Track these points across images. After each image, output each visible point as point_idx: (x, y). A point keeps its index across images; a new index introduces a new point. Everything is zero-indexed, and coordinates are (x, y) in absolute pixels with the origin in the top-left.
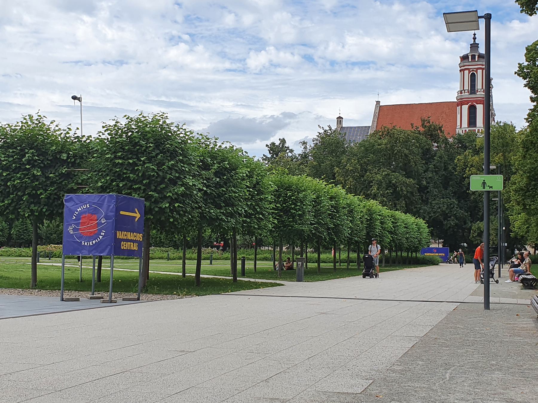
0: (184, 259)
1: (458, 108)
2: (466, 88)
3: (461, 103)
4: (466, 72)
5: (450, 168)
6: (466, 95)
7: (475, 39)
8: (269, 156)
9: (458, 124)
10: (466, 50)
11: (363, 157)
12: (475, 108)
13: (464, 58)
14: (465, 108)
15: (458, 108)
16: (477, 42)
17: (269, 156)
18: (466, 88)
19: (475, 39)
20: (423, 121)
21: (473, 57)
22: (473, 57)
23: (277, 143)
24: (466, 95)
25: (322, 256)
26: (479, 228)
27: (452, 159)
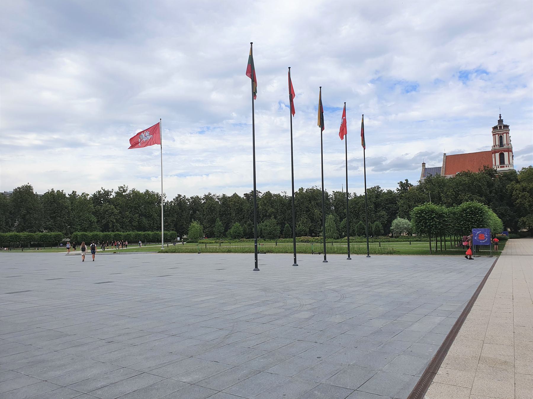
0: (368, 242)
1: (493, 155)
2: (497, 144)
3: (494, 152)
4: (497, 136)
5: (504, 191)
6: (498, 147)
7: (500, 117)
8: (400, 188)
9: (494, 163)
10: (496, 124)
11: (455, 188)
12: (503, 154)
13: (495, 128)
14: (497, 155)
15: (493, 155)
16: (502, 119)
17: (400, 188)
18: (497, 144)
19: (500, 117)
20: (485, 167)
21: (500, 127)
22: (500, 127)
23: (404, 182)
24: (498, 147)
25: (328, 245)
26: (523, 221)
27: (504, 186)
